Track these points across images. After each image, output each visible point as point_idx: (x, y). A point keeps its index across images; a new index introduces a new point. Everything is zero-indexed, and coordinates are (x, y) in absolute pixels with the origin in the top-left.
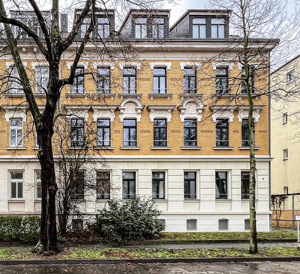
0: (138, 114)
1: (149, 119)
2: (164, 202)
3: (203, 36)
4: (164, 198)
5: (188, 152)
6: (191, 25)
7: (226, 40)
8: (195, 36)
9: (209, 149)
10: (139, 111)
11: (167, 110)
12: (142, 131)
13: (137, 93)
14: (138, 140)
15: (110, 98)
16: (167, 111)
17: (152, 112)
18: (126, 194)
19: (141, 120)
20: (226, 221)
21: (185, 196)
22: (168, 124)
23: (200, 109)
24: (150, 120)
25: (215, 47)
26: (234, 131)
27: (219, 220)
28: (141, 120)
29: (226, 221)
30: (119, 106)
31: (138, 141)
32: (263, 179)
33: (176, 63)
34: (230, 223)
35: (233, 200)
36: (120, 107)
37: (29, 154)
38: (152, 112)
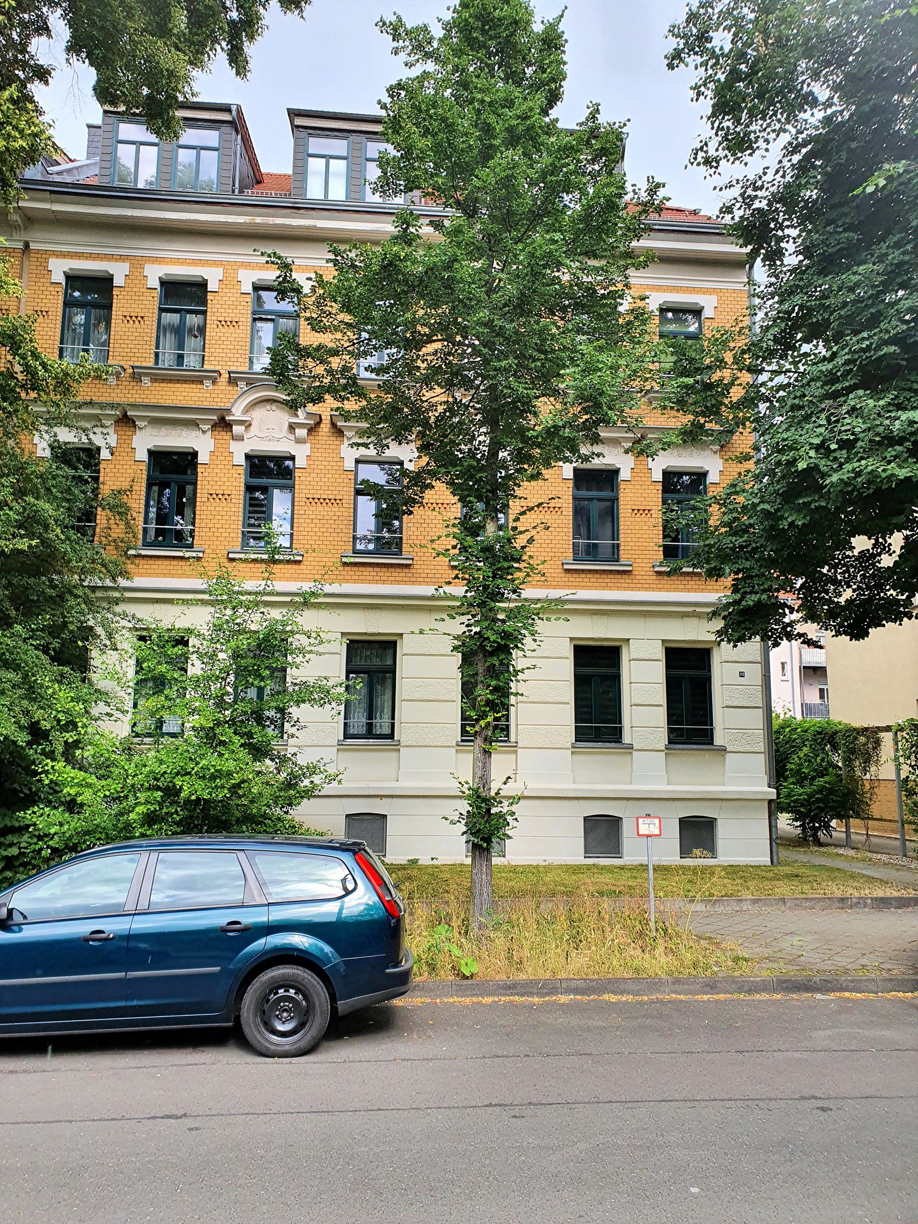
0: (298, 441)
1: (338, 459)
2: (353, 750)
3: (338, 193)
4: (391, 736)
5: (385, 573)
6: (300, 156)
7: (660, 225)
8: (314, 191)
9: (553, 570)
10: (302, 432)
11: (194, 424)
12: (312, 500)
13: (206, 367)
14: (622, 539)
15: (201, 382)
16: (195, 428)
17: (140, 428)
18: (359, 721)
19: (311, 462)
20: (614, 823)
21: (582, 735)
22: (622, 487)
23: (301, 425)
24: (230, 459)
25: (241, 219)
26: (636, 511)
27: (586, 819)
28: (311, 462)
29: (614, 823)
30: (647, 431)
31: (622, 544)
32: (742, 675)
33: (230, 268)
34: (722, 832)
35: (635, 747)
36: (229, 415)
37: (647, 586)
38: (140, 428)
